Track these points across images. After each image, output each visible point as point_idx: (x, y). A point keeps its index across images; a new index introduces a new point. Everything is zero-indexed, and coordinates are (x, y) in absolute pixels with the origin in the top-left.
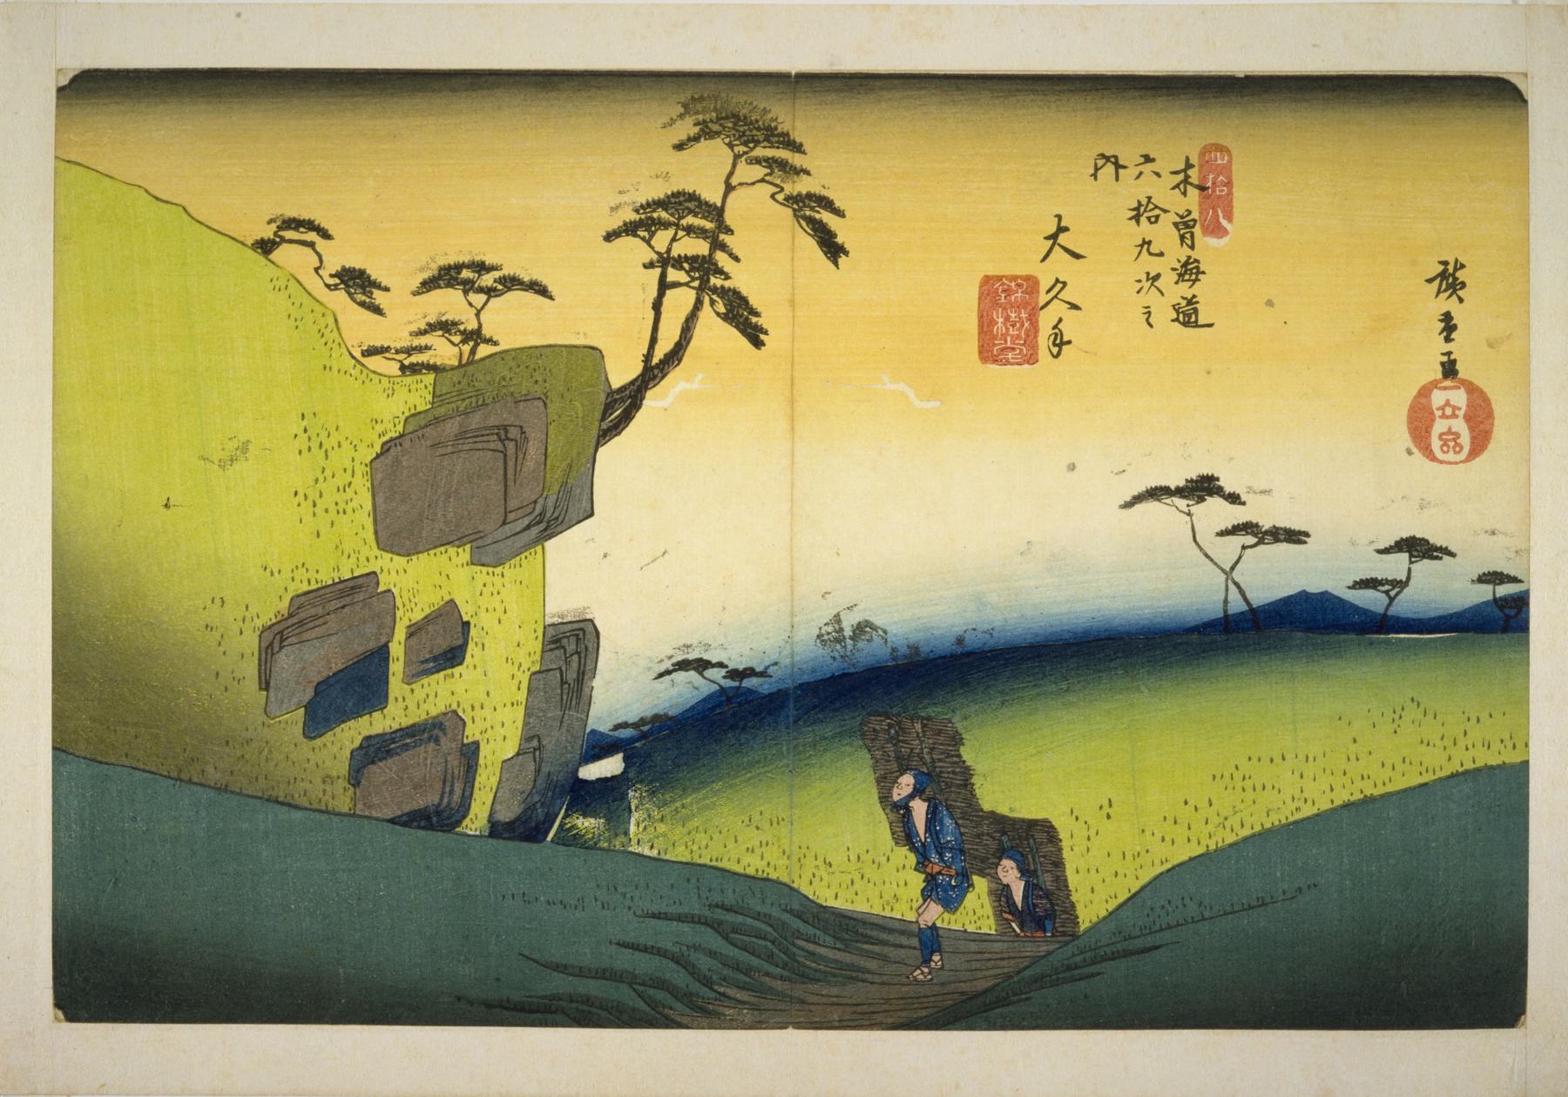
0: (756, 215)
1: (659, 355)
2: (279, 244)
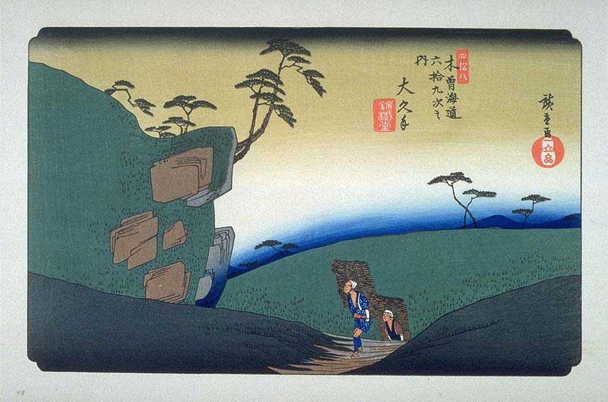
0: (293, 82)
1: (258, 127)
2: (114, 91)
